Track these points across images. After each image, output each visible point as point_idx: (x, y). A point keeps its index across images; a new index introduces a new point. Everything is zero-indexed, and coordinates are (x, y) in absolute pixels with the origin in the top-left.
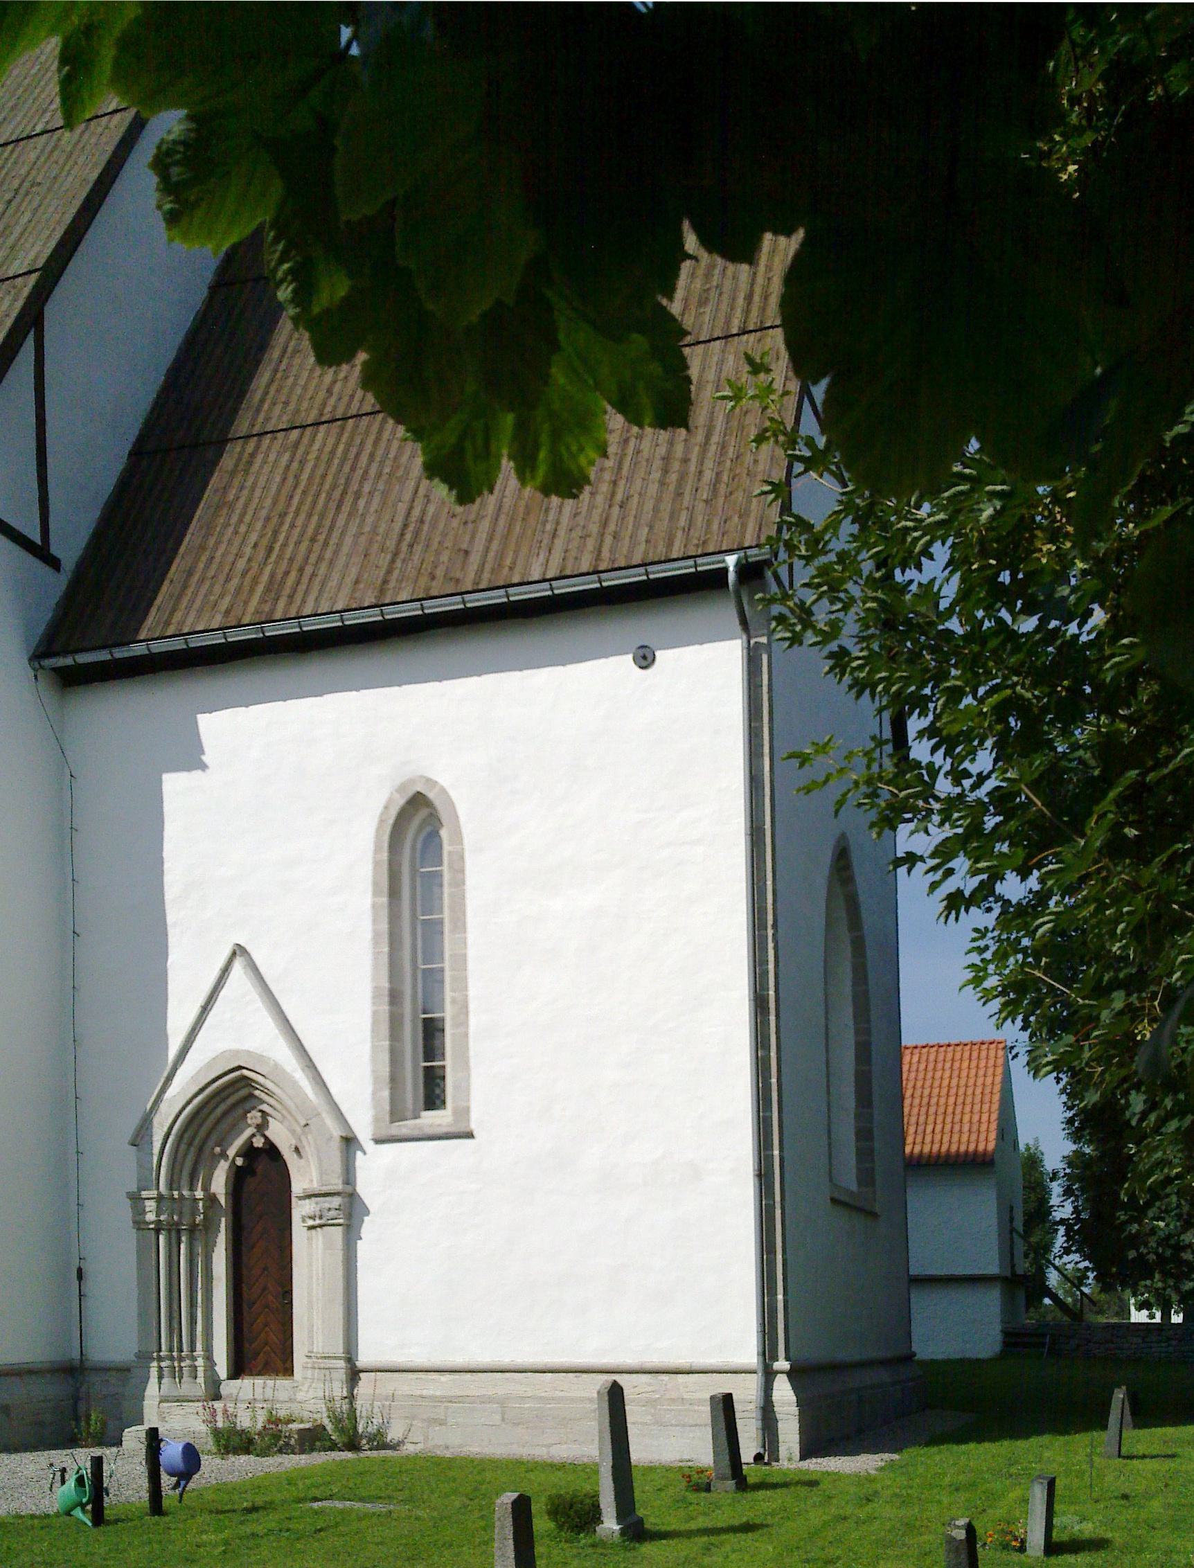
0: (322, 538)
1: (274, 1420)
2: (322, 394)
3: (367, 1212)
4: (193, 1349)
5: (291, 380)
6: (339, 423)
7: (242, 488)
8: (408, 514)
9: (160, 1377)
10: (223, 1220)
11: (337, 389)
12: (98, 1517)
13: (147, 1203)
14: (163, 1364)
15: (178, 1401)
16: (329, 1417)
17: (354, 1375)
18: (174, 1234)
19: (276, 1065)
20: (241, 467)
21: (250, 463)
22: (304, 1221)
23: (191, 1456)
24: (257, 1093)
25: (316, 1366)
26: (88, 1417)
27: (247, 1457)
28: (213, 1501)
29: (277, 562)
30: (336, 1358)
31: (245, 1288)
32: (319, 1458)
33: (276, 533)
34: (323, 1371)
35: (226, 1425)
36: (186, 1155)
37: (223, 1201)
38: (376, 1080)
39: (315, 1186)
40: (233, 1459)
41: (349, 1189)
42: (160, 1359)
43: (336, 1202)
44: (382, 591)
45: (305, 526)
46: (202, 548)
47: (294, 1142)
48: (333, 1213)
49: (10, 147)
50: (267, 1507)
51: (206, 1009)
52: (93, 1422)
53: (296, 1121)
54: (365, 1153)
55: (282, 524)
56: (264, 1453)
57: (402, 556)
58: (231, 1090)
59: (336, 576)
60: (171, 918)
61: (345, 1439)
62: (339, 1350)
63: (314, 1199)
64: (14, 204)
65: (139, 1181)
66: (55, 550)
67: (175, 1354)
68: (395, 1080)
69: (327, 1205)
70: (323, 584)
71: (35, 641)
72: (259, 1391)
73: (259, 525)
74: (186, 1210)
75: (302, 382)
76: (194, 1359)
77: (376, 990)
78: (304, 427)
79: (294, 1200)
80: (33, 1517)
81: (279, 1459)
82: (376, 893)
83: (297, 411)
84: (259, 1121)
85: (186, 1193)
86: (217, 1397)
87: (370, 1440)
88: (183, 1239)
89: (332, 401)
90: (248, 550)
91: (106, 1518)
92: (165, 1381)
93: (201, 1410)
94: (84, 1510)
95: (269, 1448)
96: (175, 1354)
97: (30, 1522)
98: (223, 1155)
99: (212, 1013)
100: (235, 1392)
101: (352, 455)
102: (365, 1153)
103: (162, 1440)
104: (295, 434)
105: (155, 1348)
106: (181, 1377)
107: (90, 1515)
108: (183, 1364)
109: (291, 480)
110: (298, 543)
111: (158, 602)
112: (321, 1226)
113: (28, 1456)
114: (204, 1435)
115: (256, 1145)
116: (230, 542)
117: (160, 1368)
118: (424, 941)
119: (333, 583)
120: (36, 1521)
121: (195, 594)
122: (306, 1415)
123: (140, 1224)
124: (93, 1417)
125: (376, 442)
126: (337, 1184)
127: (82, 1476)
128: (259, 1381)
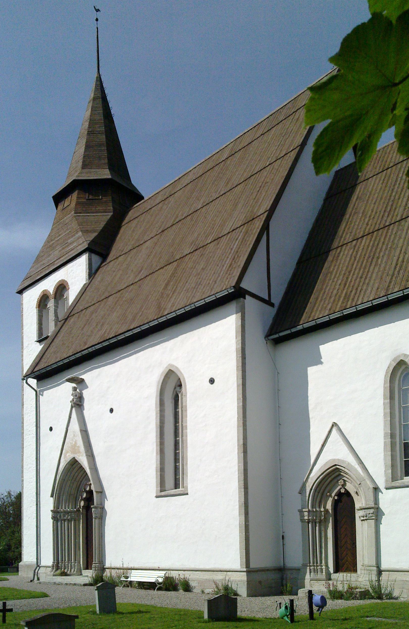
0: (364, 276)
1: (351, 588)
2: (365, 225)
3: (384, 514)
4: (321, 563)
5: (353, 224)
6: (371, 234)
7: (335, 266)
8: (398, 260)
9: (310, 572)
10: (331, 518)
11: (370, 223)
12: (292, 620)
13: (305, 513)
14: (311, 568)
15: (316, 580)
16: (371, 587)
17: (380, 572)
18: (314, 523)
19: (349, 463)
20: (335, 258)
21: (338, 256)
22: (360, 518)
23: (323, 599)
24: (342, 473)
25: (366, 569)
26: (287, 586)
27: (341, 600)
28: (331, 616)
29: (348, 289)
30: (374, 566)
31: (339, 542)
32: (368, 602)
33: (347, 278)
34: (368, 571)
35: (334, 589)
36: (317, 496)
37: (331, 512)
38: (386, 466)
39: (364, 506)
40: (336, 601)
41: (376, 506)
42: (310, 566)
43: (372, 511)
44: (387, 290)
45: (358, 273)
46: (321, 289)
47: (355, 490)
48: (370, 515)
49: (258, 173)
50: (350, 619)
51: (323, 446)
52: (288, 587)
53: (356, 482)
54: (382, 493)
55: (349, 275)
56: (347, 599)
57: (395, 276)
58: (333, 473)
59: (370, 289)
60: (311, 416)
61: (377, 595)
62: (374, 563)
63: (363, 510)
64: (260, 191)
65: (302, 506)
66: (272, 301)
67: (315, 564)
68: (393, 466)
69: (368, 512)
70: (365, 292)
71: (266, 331)
72: (345, 577)
73: (341, 277)
74: (318, 515)
75: (357, 223)
76: (322, 566)
77: (385, 434)
78: (358, 239)
79: (356, 511)
80: (271, 619)
81: (353, 601)
82: (384, 399)
83: (356, 234)
84: (343, 483)
85: (318, 509)
86: (330, 579)
87: (387, 595)
88: (317, 525)
89: (368, 228)
90: (337, 287)
91: (295, 620)
92: (312, 573)
93: (325, 584)
94: (288, 617)
95: (349, 597)
96: (315, 564)
97: (270, 620)
98: (330, 496)
99: (325, 447)
100: (336, 578)
101: (376, 244)
102: (382, 493)
103: (313, 594)
104: (355, 242)
105: (309, 563)
106: (317, 573)
107: (290, 619)
108: (318, 568)
109: (353, 258)
110: (356, 280)
111: (306, 310)
112: (366, 520)
113: (267, 598)
114: (326, 592)
115: (342, 492)
116: (331, 285)
117: (310, 569)
118: (404, 413)
119: (368, 291)
120: (272, 620)
121: (319, 305)
122: (362, 586)
123: (302, 520)
124: (288, 585)
125: (385, 239)
126: (372, 504)
127: (287, 606)
128: (345, 574)
